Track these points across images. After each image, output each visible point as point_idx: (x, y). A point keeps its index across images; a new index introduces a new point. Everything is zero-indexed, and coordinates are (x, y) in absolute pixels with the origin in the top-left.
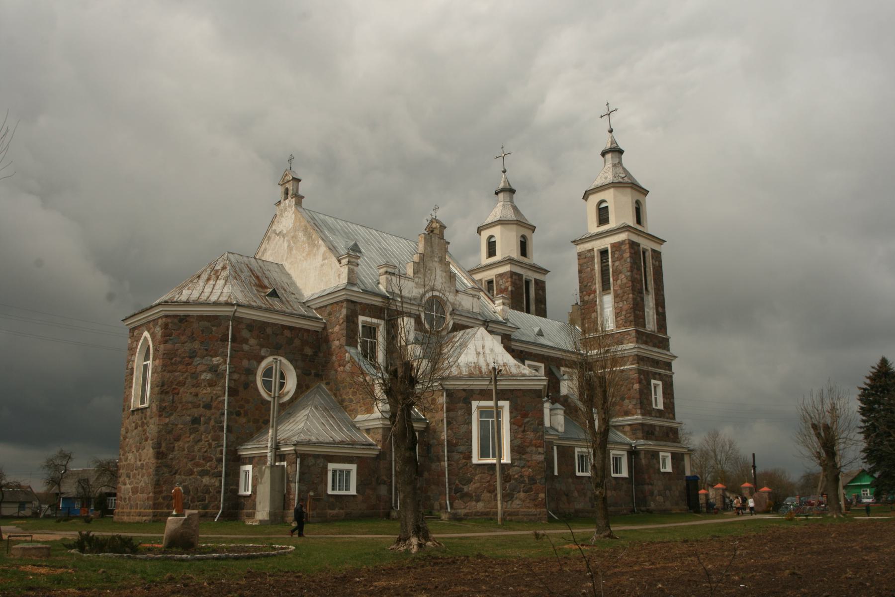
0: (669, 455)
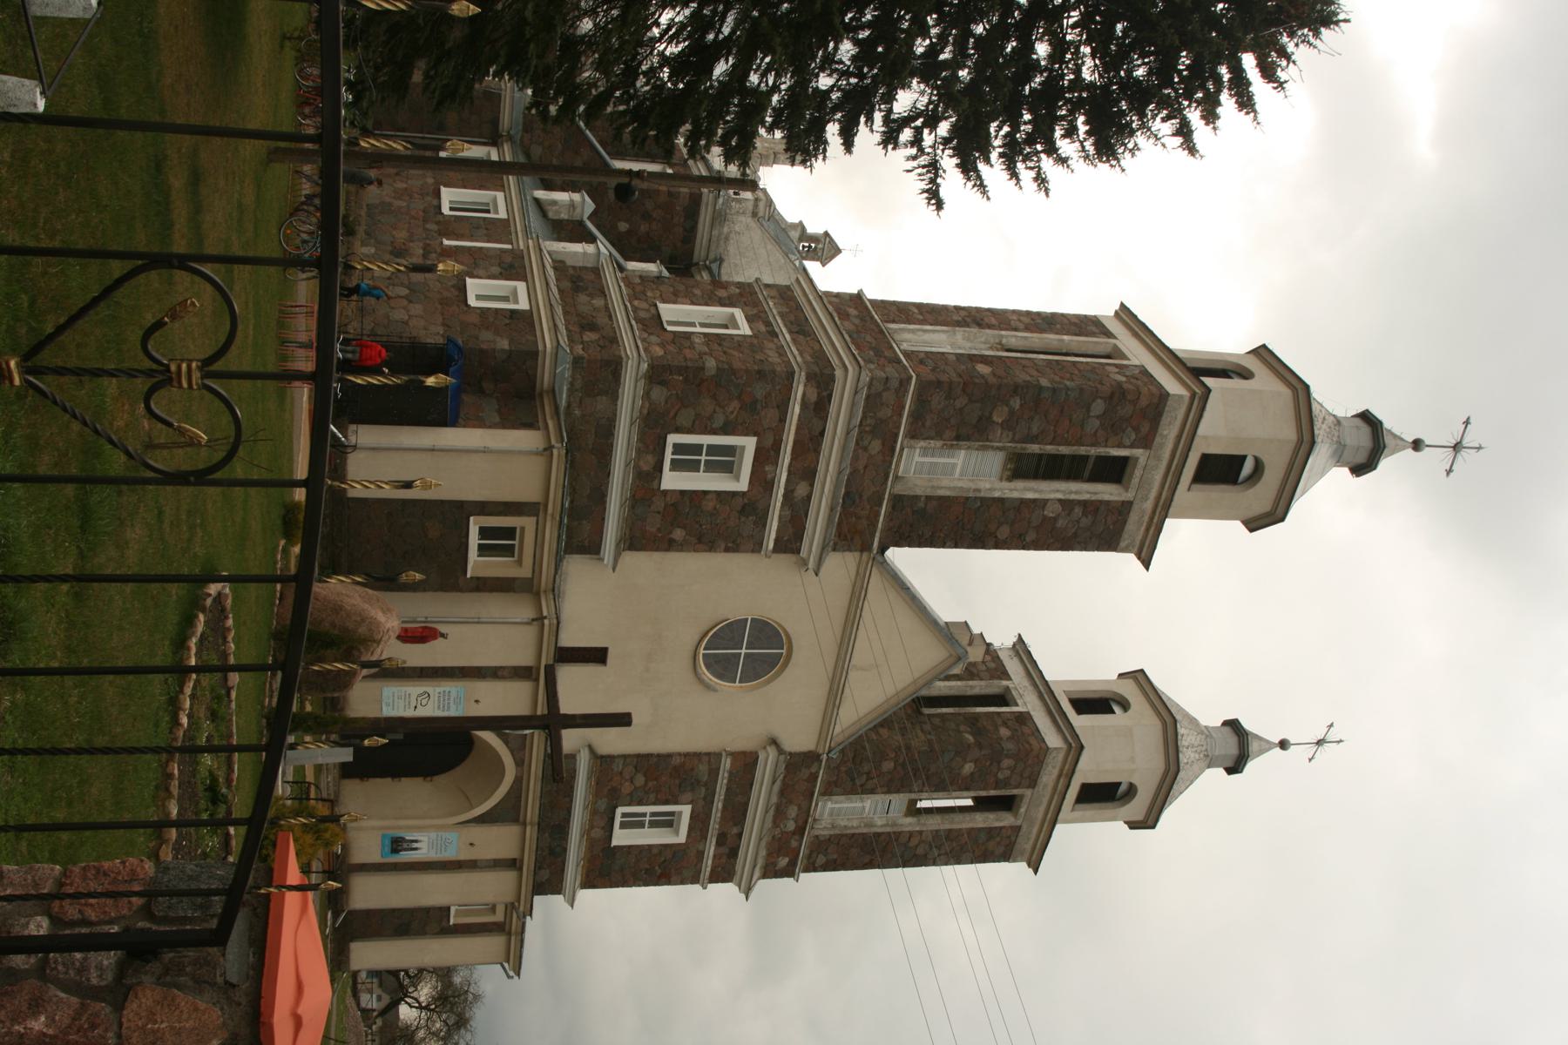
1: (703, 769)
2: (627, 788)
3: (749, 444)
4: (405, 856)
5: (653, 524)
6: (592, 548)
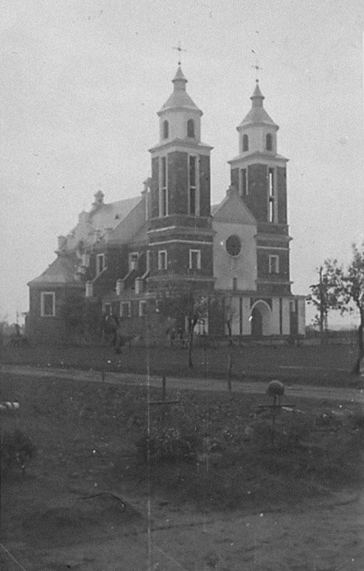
3: (191, 251)
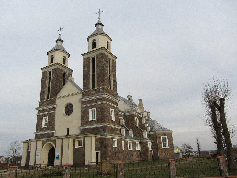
0: (117, 140)
1: (83, 109)
2: (86, 120)
4: (60, 157)
5: (51, 127)
6: (53, 133)
